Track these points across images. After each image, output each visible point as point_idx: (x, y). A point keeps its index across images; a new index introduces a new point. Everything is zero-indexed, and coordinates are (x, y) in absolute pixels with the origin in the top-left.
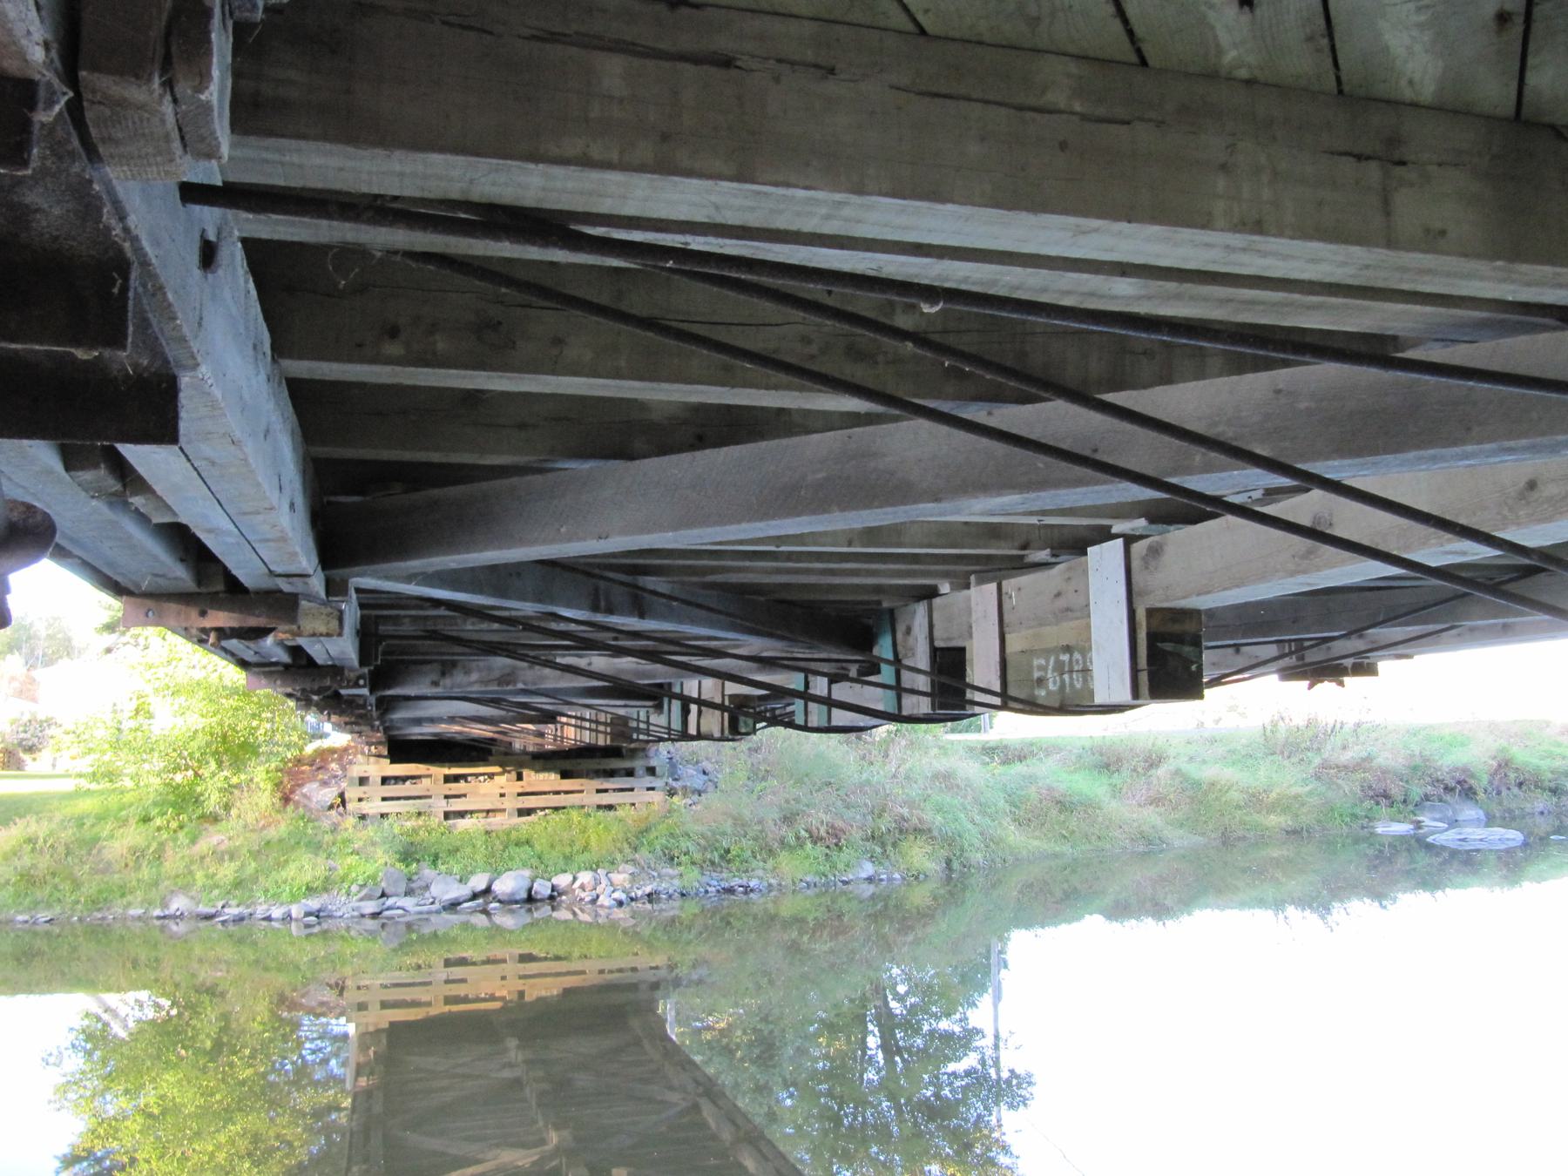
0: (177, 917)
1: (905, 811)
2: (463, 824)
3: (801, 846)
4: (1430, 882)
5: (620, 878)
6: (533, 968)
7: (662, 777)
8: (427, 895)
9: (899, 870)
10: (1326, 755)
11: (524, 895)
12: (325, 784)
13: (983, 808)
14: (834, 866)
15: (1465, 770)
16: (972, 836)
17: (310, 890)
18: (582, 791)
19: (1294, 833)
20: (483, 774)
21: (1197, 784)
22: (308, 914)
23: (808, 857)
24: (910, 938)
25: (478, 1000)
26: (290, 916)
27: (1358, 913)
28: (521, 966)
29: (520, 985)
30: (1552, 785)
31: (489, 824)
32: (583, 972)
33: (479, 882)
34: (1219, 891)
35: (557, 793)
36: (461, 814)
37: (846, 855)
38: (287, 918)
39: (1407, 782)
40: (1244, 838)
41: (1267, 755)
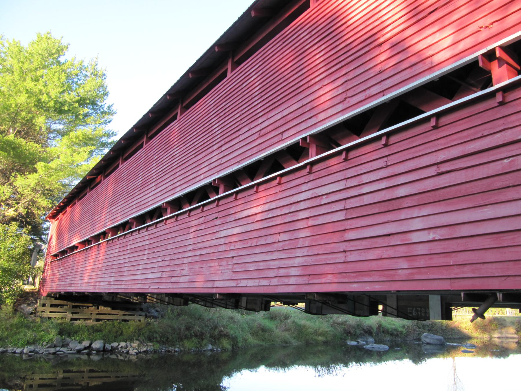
1: (222, 329)
2: (77, 323)
3: (191, 338)
4: (360, 360)
5: (135, 344)
6: (94, 374)
7: (144, 312)
8: (68, 347)
9: (219, 348)
10: (334, 319)
11: (102, 349)
12: (29, 305)
13: (242, 329)
14: (201, 345)
15: (370, 327)
16: (240, 339)
17: (29, 343)
18: (117, 314)
19: (325, 343)
21: (299, 326)
22: (30, 352)
23: (193, 342)
24: (220, 370)
25: (72, 385)
27: (340, 370)
29: (87, 380)
30: (391, 333)
31: (86, 323)
32: (110, 377)
33: (86, 343)
34: (303, 360)
35: (109, 314)
36: (76, 319)
37: (204, 342)
38: (22, 353)
39: (356, 329)
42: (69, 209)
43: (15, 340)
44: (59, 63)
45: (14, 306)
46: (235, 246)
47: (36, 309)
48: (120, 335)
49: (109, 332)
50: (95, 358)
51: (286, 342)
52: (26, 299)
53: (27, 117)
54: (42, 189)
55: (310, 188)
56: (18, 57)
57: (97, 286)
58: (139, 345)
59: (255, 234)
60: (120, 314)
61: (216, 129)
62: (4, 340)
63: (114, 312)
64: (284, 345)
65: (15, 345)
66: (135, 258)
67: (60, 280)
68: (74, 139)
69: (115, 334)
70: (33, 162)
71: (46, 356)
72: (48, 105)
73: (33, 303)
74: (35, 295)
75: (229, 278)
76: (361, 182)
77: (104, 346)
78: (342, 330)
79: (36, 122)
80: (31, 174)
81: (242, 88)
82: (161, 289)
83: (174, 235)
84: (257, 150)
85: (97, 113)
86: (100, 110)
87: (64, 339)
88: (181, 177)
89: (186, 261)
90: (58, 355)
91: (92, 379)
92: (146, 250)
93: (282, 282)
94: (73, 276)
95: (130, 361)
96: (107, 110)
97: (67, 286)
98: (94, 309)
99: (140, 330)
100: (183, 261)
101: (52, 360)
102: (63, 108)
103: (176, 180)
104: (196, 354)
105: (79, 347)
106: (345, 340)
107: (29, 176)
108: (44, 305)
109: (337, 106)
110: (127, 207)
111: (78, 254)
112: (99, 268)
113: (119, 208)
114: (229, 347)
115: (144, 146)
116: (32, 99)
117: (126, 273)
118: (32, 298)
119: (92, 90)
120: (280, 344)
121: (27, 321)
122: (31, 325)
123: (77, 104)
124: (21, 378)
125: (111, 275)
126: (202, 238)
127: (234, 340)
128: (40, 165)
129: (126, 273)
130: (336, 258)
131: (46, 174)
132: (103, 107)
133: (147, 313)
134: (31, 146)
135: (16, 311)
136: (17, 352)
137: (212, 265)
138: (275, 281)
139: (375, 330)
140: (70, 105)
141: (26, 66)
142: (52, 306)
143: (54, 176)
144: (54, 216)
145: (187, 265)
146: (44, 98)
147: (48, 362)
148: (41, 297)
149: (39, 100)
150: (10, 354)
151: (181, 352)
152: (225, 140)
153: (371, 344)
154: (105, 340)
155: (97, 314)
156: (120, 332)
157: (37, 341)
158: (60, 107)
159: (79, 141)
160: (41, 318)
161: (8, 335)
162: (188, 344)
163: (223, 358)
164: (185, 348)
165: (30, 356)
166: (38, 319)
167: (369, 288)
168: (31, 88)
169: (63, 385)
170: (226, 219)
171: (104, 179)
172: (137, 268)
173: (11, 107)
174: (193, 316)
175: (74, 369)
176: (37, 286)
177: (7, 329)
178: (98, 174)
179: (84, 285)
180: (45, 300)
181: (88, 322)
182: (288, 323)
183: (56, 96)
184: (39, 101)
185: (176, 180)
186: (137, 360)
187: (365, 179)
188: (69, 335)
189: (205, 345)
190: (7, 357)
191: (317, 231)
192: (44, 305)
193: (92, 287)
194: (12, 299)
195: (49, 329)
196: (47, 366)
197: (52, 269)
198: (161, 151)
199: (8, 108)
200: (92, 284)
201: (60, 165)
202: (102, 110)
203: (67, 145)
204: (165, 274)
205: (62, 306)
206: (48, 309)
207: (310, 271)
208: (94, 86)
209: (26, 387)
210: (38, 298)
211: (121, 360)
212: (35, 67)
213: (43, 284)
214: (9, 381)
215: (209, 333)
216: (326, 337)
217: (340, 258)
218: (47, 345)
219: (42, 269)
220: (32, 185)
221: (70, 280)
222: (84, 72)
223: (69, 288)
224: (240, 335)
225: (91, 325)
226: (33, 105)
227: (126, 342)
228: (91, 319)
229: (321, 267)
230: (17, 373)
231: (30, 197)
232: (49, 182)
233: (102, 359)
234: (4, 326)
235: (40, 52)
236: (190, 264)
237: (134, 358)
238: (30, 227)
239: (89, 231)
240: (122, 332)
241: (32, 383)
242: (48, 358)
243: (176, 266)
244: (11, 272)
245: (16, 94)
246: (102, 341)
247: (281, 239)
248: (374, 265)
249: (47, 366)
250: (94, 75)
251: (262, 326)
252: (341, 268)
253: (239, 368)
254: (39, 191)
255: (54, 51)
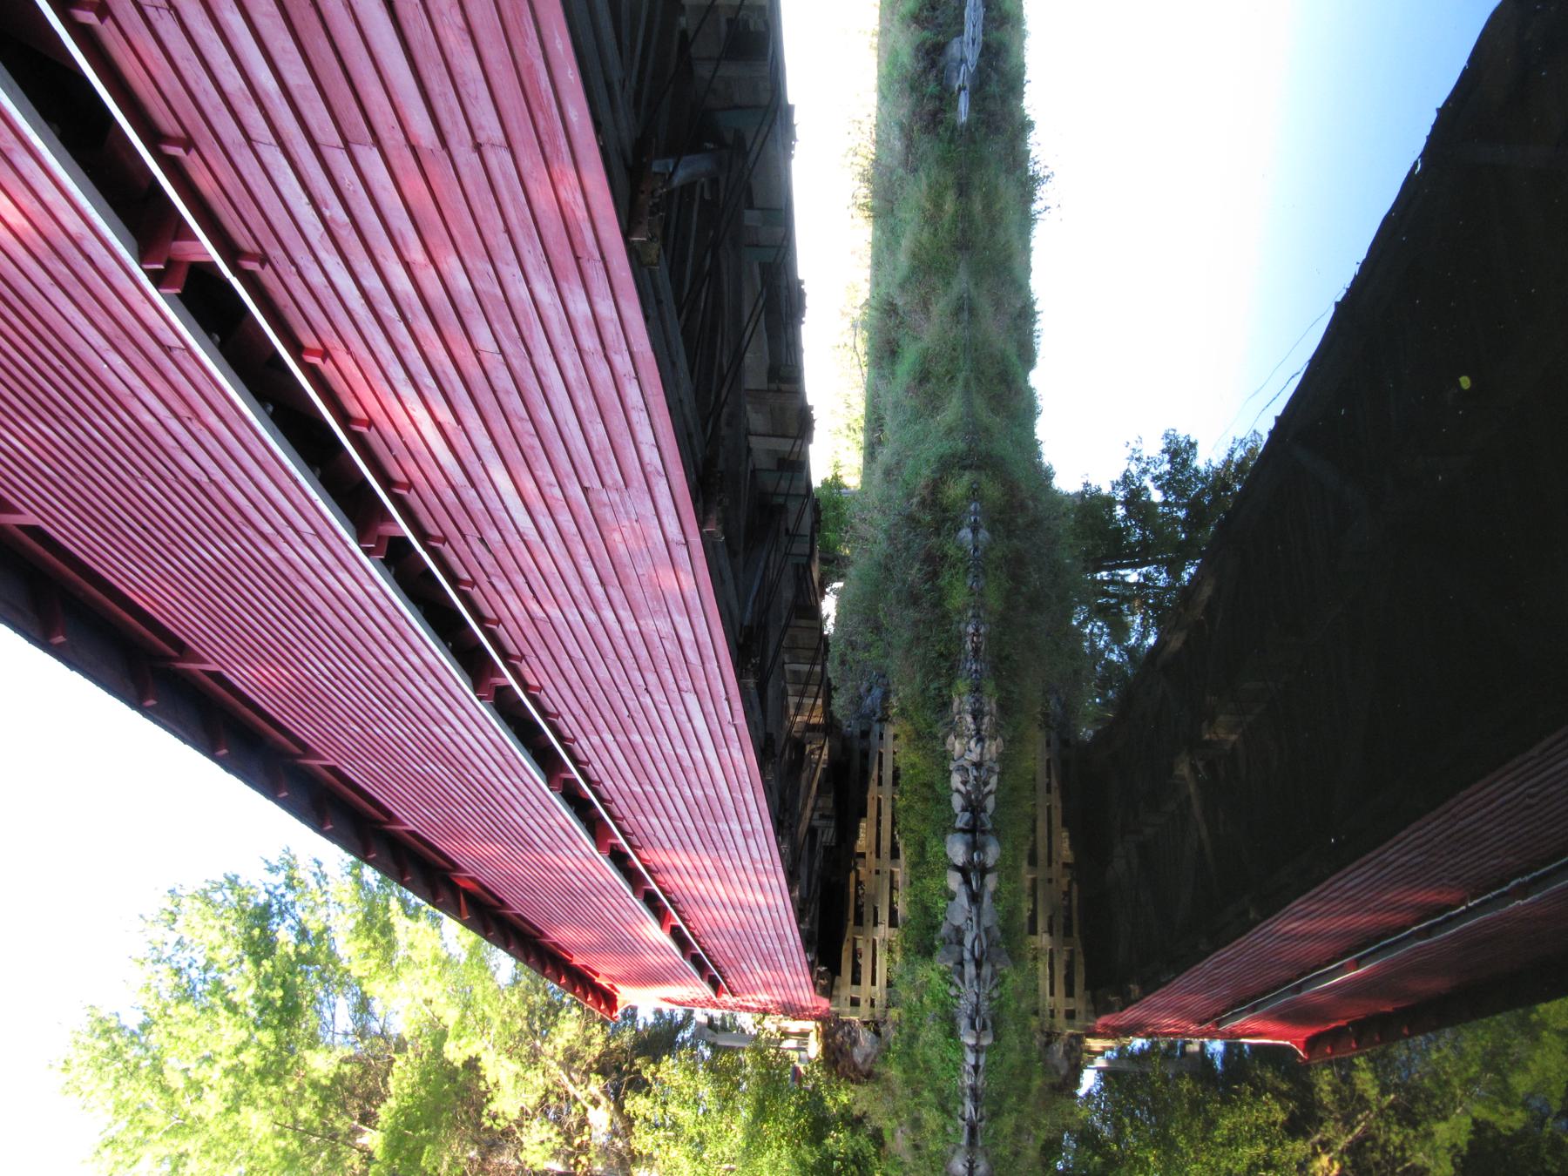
0: (971, 1165)
1: (915, 500)
2: (902, 909)
3: (941, 589)
4: (1013, 85)
5: (956, 746)
6: (1042, 851)
7: (871, 727)
8: (964, 927)
11: (968, 837)
12: (855, 1042)
13: (918, 441)
16: (945, 447)
17: (953, 1033)
19: (963, 190)
20: (857, 891)
21: (914, 270)
22: (973, 1026)
23: (950, 583)
24: (1030, 503)
26: (974, 1046)
27: (1043, 148)
28: (1040, 863)
29: (1057, 867)
31: (904, 883)
32: (1049, 808)
33: (954, 881)
34: (1009, 257)
36: (893, 913)
37: (951, 550)
38: (977, 1049)
39: (924, 96)
40: (964, 231)
41: (893, 215)
42: (578, 961)
43: (943, 1069)
44: (144, 1027)
45: (858, 1083)
46: (551, 485)
47: (866, 1023)
48: (934, 791)
49: (925, 819)
50: (992, 853)
51: (958, 311)
52: (840, 1050)
53: (315, 1103)
54: (530, 1038)
55: (312, 258)
56: (131, 1146)
57: (767, 866)
58: (959, 736)
59: (500, 427)
60: (880, 795)
61: (215, 552)
62: (946, 1098)
63: (872, 811)
64: (965, 315)
65: (956, 1069)
66: (660, 770)
67: (777, 968)
68: (372, 963)
69: (931, 803)
70: (451, 1074)
71: (985, 983)
72: (272, 1047)
73: (849, 1033)
74: (830, 1027)
75: (648, 497)
76: (244, 94)
77: (963, 831)
78: (925, 138)
79: (326, 1076)
80: (482, 1073)
81: (61, 476)
82: (730, 691)
83: (566, 664)
84: (242, 427)
85: (293, 903)
86: (283, 896)
87: (943, 940)
88: (392, 650)
89: (631, 626)
90: (982, 953)
91: (1054, 856)
92: (632, 738)
93: (618, 338)
94: (757, 932)
95: (1002, 758)
96: (282, 874)
97: (786, 946)
98: (864, 866)
99: (919, 735)
100: (635, 632)
101: (998, 967)
102: (279, 1003)
103: (405, 665)
104: (985, 572)
105: (963, 899)
106: (955, 128)
107: (490, 1080)
108: (855, 1002)
109: (25, 172)
110: (522, 799)
111: (691, 924)
112: (716, 864)
113: (531, 821)
114: (967, 477)
115: (333, 762)
116: (255, 1093)
117: (711, 792)
118: (839, 1036)
119: (218, 924)
120: (964, 328)
121: (896, 1044)
122: (906, 1031)
123: (265, 962)
124: (1048, 1044)
125: (725, 831)
126: (552, 582)
127: (948, 465)
128: (455, 1053)
129: (711, 792)
130: (504, 175)
131: (482, 1032)
132: (271, 888)
133: (875, 718)
134: (402, 1080)
135: (870, 1076)
136: (973, 1063)
137: (622, 548)
138: (622, 363)
139: (926, 34)
140: (268, 982)
141: (158, 1119)
142: (856, 981)
143: (486, 1008)
144: (607, 998)
145: (642, 622)
146: (251, 1059)
147: (1004, 978)
148: (834, 1012)
149: (257, 1072)
150: (981, 1078)
151: (979, 616)
152: (240, 525)
153: (965, 50)
154: (945, 833)
155: (878, 856)
156: (924, 790)
157: (947, 1011)
158: (278, 1011)
159: (375, 949)
160: (888, 1007)
161: (932, 1090)
162: (958, 598)
163: (997, 494)
164: (966, 607)
165: (984, 1027)
166: (893, 1013)
167: (570, 72)
168: (221, 1101)
169: (1068, 932)
170: (479, 513)
171: (463, 871)
172: (687, 762)
173: (285, 1150)
174: (881, 587)
175: (1026, 905)
176: (810, 1025)
177: (916, 1093)
178: (454, 888)
179: (771, 901)
180: (842, 998)
181: (899, 878)
182: (906, 303)
183: (242, 1026)
184: (262, 1074)
185: (405, 665)
186: (999, 740)
187: (232, 81)
188: (935, 927)
189: (959, 548)
190: (989, 1085)
191: (437, 236)
192: (855, 1002)
193: (774, 881)
194: (839, 1088)
195: (917, 983)
196: (1014, 979)
197: (753, 990)
198: (329, 713)
199: (289, 1157)
200: (764, 879)
201: (449, 998)
202: (282, 890)
203: (391, 980)
204: (686, 684)
205: (856, 954)
206: (865, 990)
207: (564, 258)
208: (206, 920)
209: (1073, 1027)
210: (838, 1021)
211: (999, 781)
212: (160, 1095)
213: (797, 1011)
214: (1057, 1072)
215: (927, 539)
216: (946, 188)
217: (499, 160)
218: (957, 986)
219: (758, 1016)
220: (516, 1066)
221: (768, 940)
222: (168, 951)
223: (792, 942)
224: (937, 446)
225: (908, 870)
226: (275, 1088)
227: (950, 773)
228: (892, 873)
229: (543, 222)
230: (1034, 1055)
231: (557, 1072)
232: (504, 1022)
233: (996, 832)
234: (909, 1101)
235: (111, 1084)
236: (637, 613)
237: (993, 748)
238: (639, 1061)
239: (620, 900)
240: (925, 785)
241: (1063, 1014)
242: (992, 979)
243: (653, 653)
244: (764, 1100)
245: (243, 1140)
246: (949, 837)
247: (493, 347)
248: (495, 53)
249: (1014, 979)
250: (175, 921)
251: (913, 384)
252: (530, 160)
253: (1031, 447)
254: (534, 1047)
255: (104, 1045)
